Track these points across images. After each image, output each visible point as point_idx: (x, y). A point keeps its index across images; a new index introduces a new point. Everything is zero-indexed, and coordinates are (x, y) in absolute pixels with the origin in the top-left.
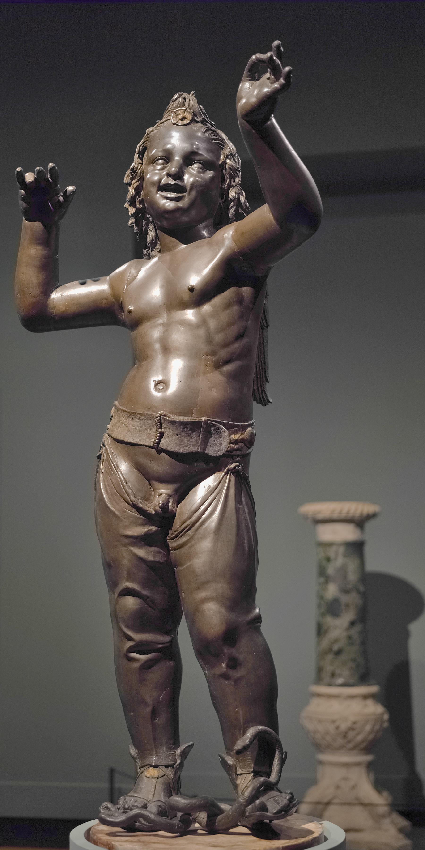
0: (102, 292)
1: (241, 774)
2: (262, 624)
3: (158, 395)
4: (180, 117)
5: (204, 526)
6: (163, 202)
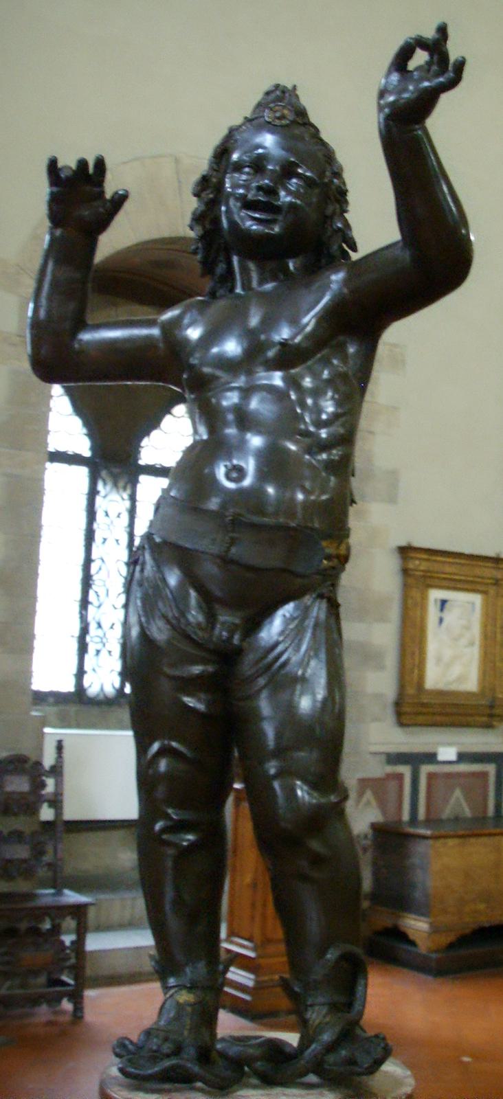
0: (149, 338)
1: (311, 1006)
2: (347, 176)
3: (231, 485)
4: (278, 114)
5: (283, 672)
6: (249, 223)
